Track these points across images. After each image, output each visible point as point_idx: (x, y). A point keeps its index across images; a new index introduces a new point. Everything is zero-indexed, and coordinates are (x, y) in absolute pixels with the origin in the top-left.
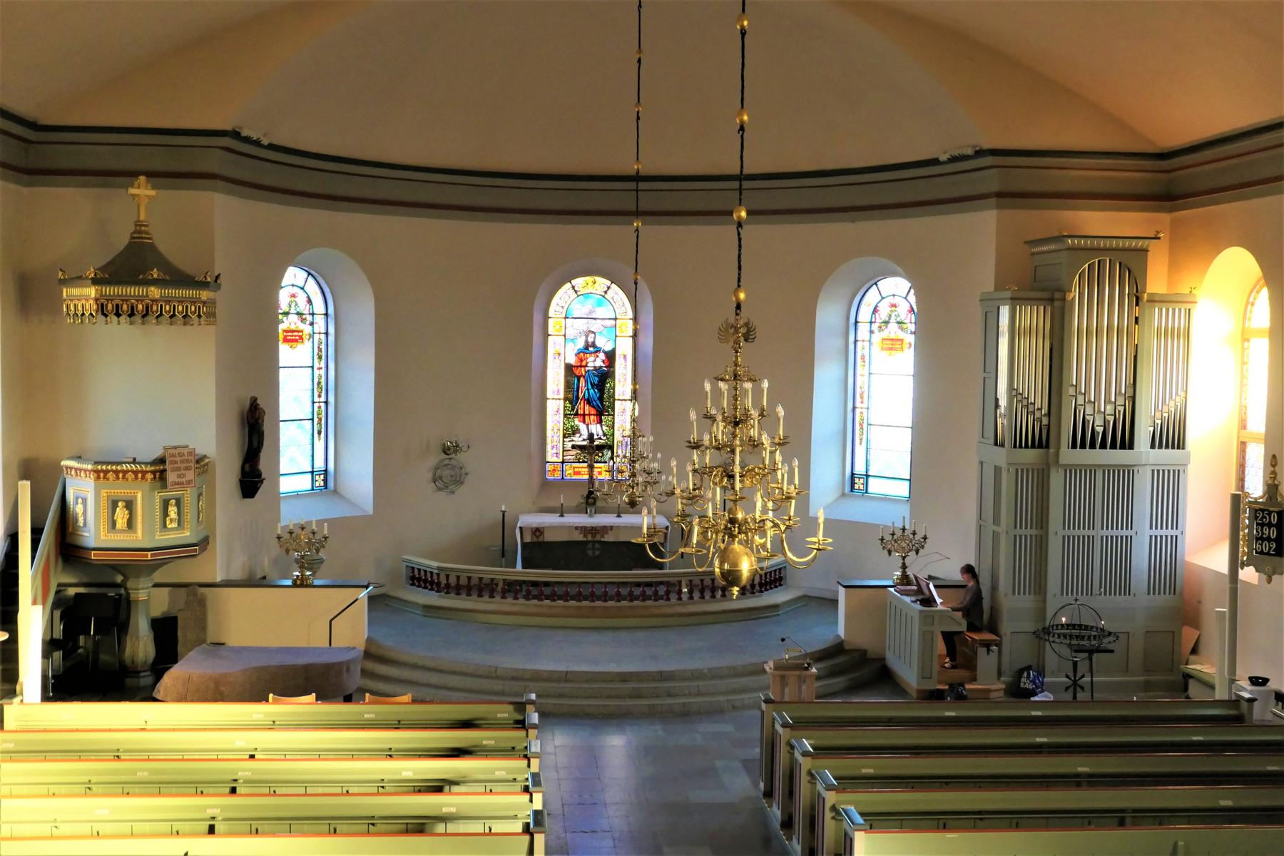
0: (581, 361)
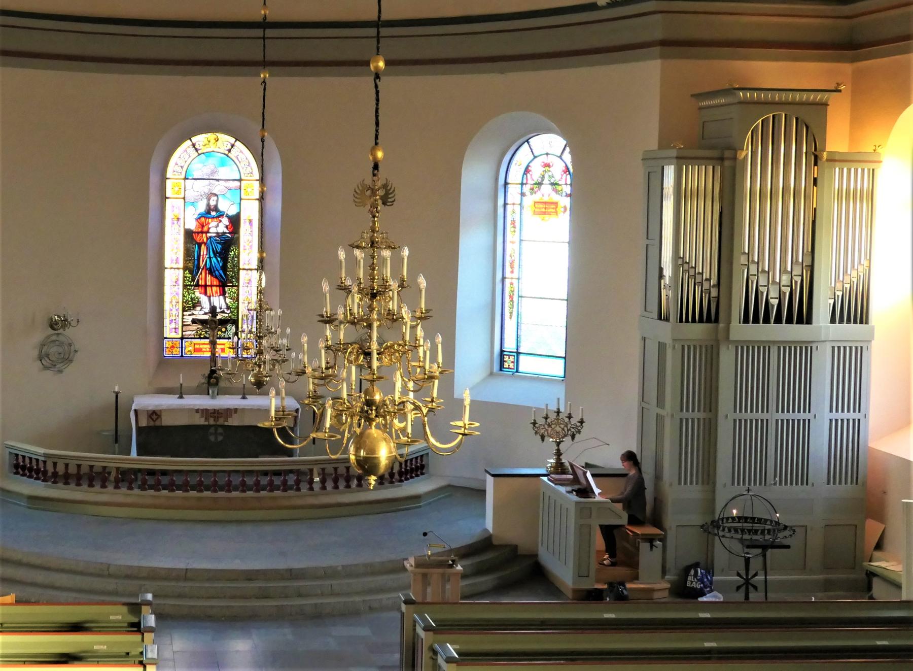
0: (203, 226)
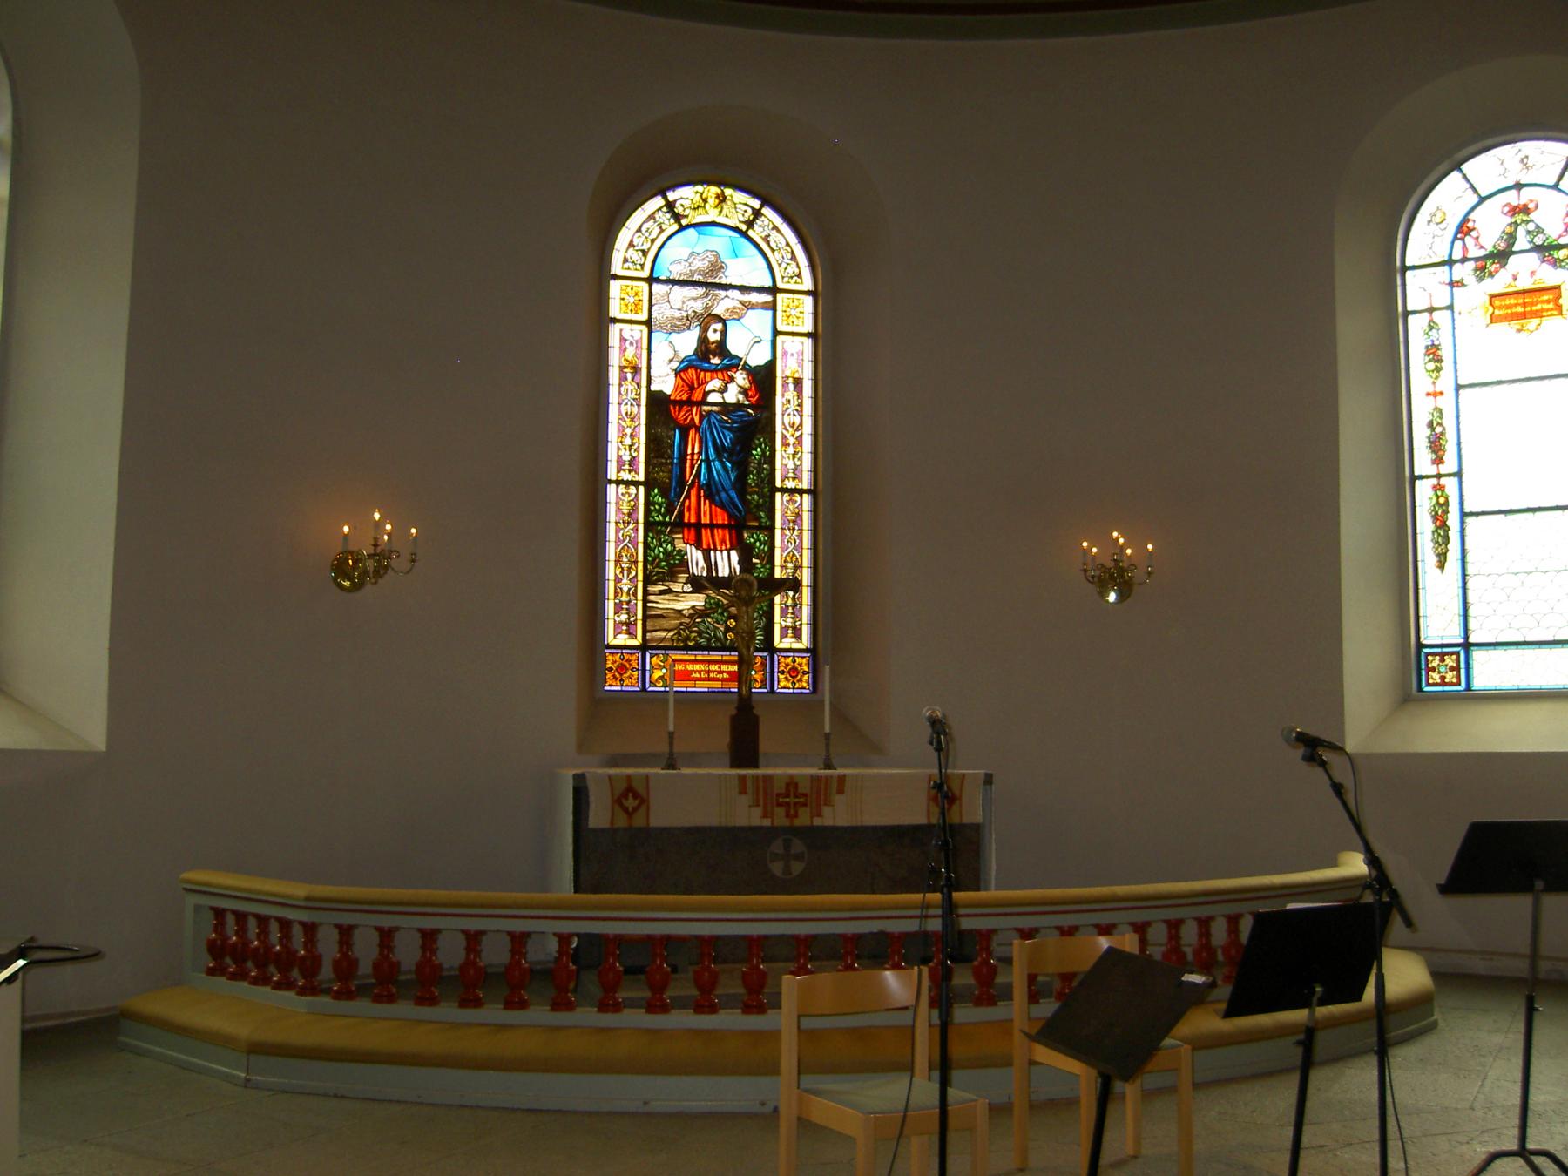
0: (692, 389)
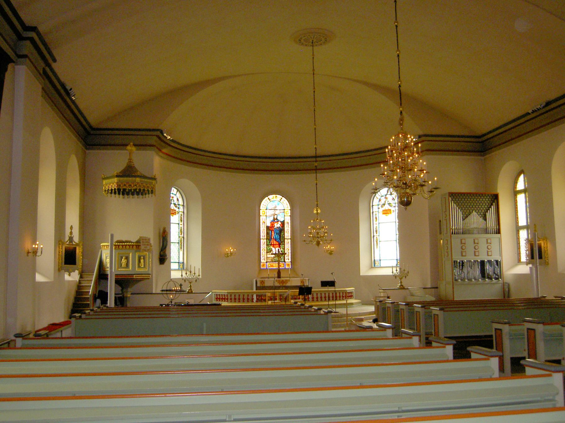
0: (272, 225)
